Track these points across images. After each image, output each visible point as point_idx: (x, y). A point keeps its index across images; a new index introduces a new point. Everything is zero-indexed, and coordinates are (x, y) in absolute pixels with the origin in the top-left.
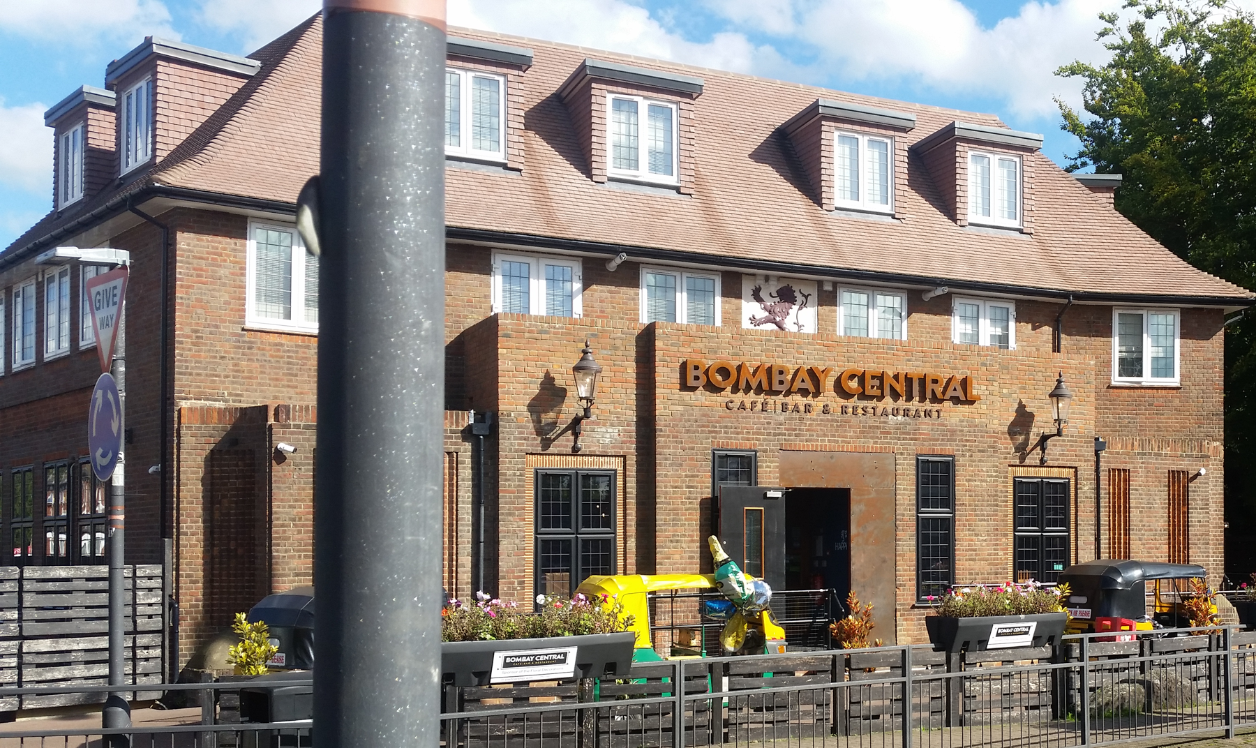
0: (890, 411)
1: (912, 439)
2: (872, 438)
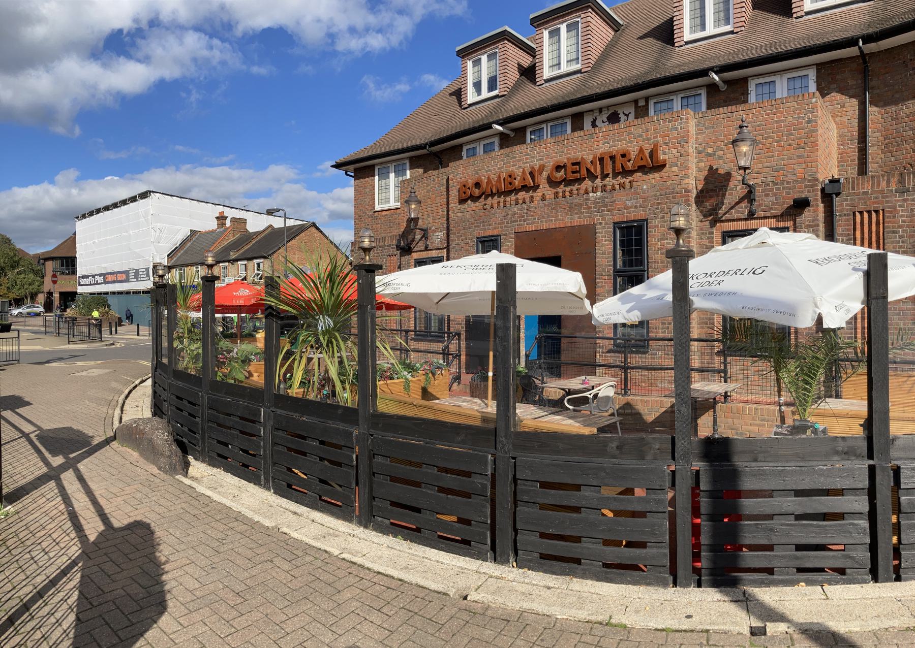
0: (590, 189)
1: (609, 210)
2: (577, 214)
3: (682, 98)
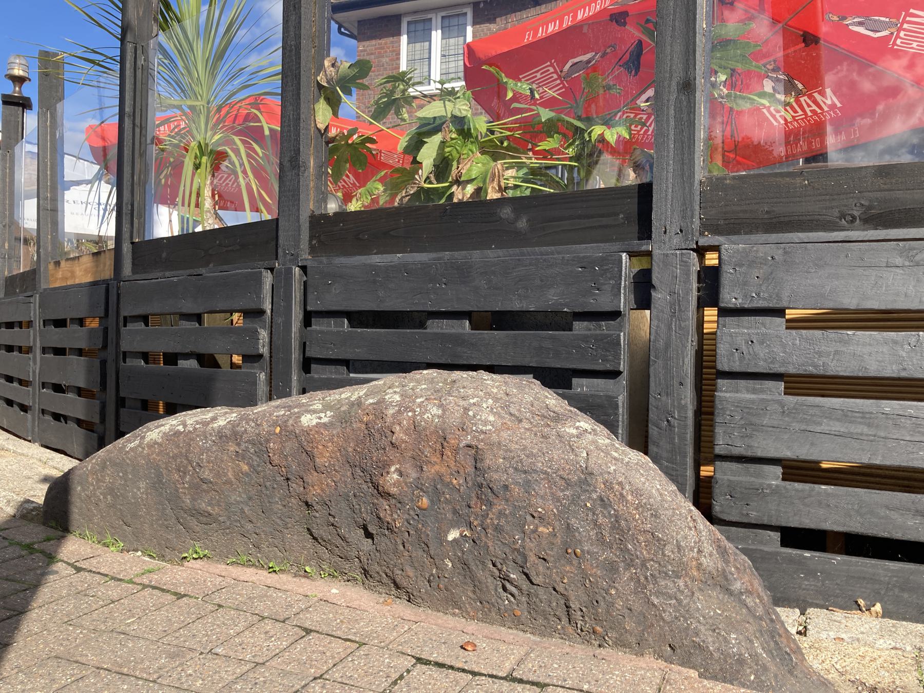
3: (443, 17)
